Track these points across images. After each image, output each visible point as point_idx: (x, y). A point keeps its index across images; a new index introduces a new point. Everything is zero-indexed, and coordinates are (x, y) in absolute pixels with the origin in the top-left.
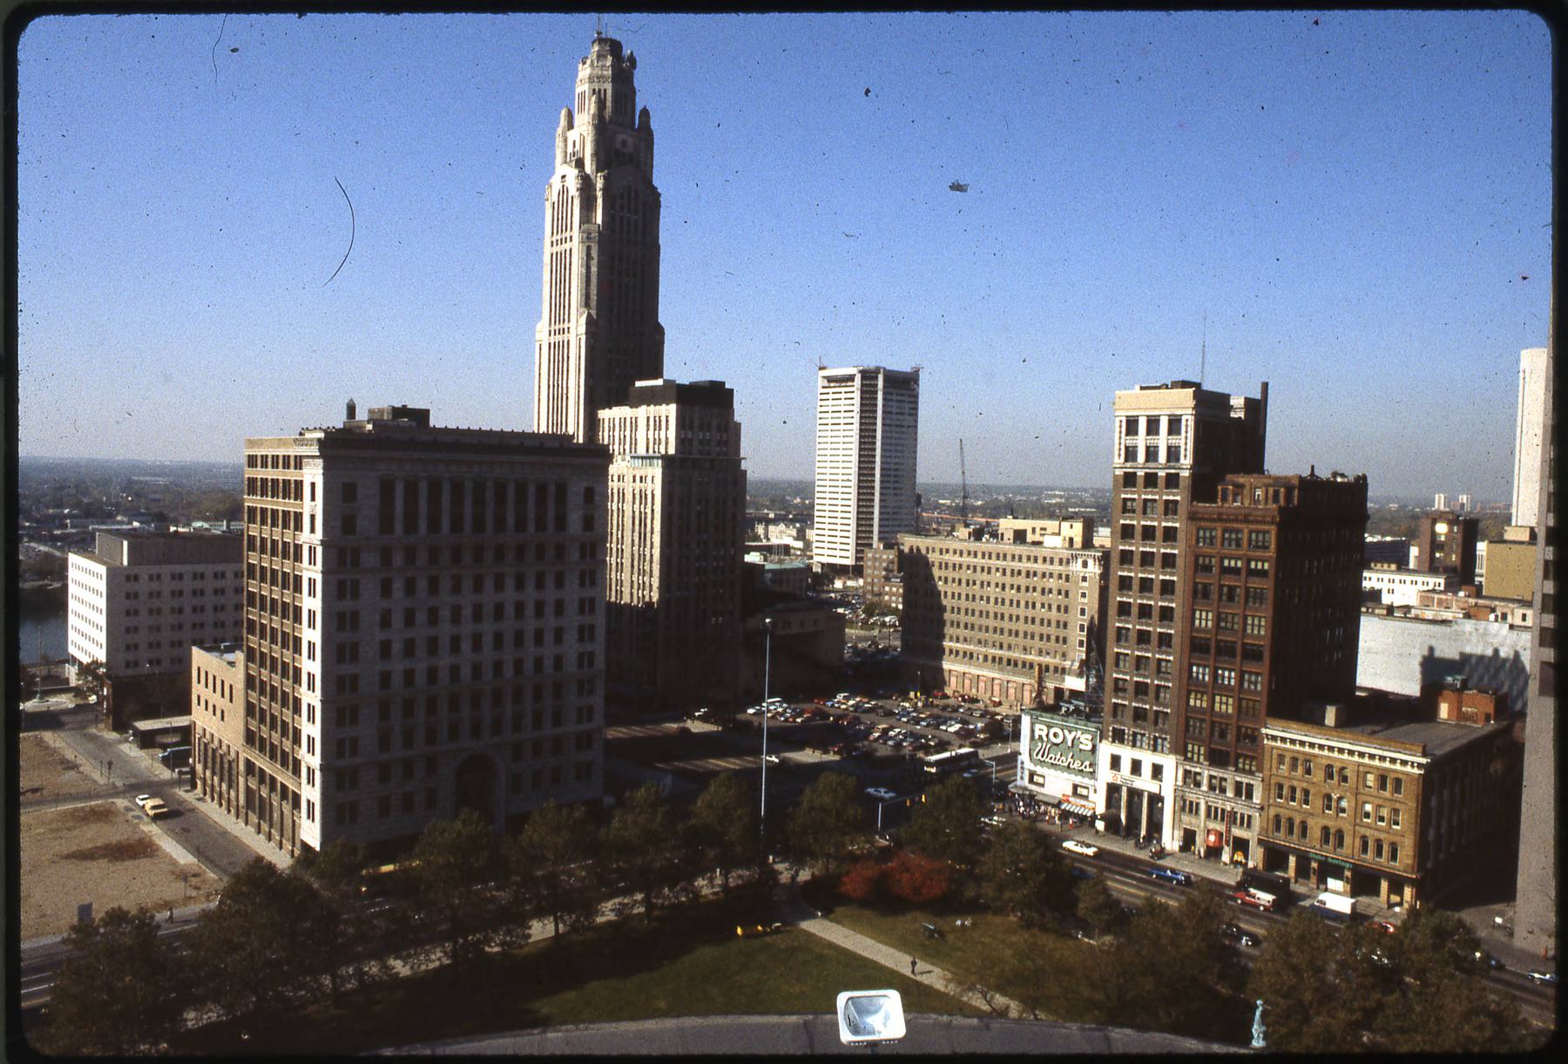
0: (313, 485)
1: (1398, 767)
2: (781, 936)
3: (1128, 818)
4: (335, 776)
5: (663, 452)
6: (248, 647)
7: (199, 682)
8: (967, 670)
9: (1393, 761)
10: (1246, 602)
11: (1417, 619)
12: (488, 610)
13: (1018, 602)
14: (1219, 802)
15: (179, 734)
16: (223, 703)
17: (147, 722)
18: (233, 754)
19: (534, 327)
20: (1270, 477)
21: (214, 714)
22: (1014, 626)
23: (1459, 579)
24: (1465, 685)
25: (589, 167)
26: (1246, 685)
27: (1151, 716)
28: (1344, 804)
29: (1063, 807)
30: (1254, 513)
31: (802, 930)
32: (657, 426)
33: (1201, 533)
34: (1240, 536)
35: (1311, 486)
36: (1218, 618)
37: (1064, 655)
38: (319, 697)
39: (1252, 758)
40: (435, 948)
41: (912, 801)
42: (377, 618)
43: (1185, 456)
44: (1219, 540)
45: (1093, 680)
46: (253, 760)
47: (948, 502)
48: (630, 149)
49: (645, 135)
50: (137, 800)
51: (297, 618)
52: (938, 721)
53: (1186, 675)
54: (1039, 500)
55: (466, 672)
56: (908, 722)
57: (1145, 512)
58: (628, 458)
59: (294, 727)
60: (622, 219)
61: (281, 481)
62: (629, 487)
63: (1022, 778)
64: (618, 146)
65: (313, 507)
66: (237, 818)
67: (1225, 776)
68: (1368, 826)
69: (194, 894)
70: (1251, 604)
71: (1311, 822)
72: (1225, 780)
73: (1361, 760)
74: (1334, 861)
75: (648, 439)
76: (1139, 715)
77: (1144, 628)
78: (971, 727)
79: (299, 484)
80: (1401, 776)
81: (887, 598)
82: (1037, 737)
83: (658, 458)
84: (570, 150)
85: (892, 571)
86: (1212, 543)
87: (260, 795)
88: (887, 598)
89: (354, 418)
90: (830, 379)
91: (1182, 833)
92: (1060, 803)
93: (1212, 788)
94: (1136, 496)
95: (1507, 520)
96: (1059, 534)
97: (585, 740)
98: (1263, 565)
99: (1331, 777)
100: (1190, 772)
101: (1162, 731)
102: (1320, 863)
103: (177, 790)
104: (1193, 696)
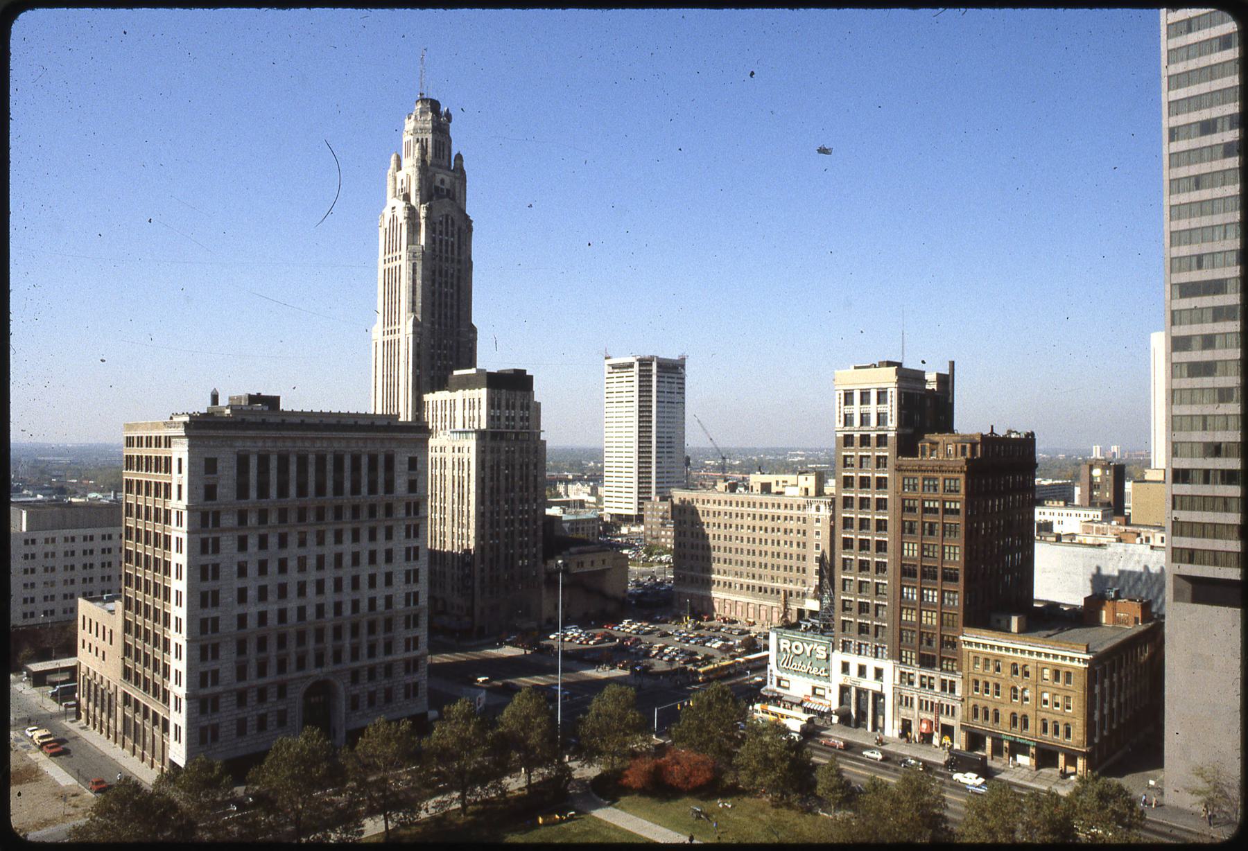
0: (180, 460)
1: (1068, 662)
2: (575, 822)
4: (200, 704)
5: (477, 427)
6: (126, 597)
7: (84, 628)
8: (727, 597)
9: (1064, 658)
10: (944, 535)
11: (1081, 544)
12: (330, 560)
13: (766, 540)
14: (928, 696)
16: (104, 645)
17: (40, 664)
20: (958, 435)
22: (763, 560)
23: (1112, 511)
24: (1118, 596)
25: (414, 201)
26: (946, 601)
27: (872, 630)
28: (1027, 694)
29: (805, 705)
30: (904, 463)
31: (593, 817)
33: (906, 482)
34: (936, 483)
35: (990, 442)
37: (804, 582)
38: (185, 638)
39: (954, 660)
41: (682, 705)
42: (235, 568)
43: (891, 420)
44: (920, 485)
46: (129, 693)
47: (712, 462)
48: (447, 186)
50: (27, 732)
51: (167, 571)
52: (704, 641)
53: (898, 594)
55: (311, 612)
56: (680, 641)
57: (861, 466)
58: (448, 432)
59: (164, 663)
60: (441, 241)
61: (153, 458)
62: (449, 456)
63: (771, 682)
64: (438, 184)
65: (179, 479)
67: (933, 675)
69: (72, 811)
70: (947, 536)
71: (1001, 710)
72: (933, 678)
73: (1039, 659)
74: (1021, 741)
75: (464, 417)
76: (863, 629)
78: (731, 643)
79: (168, 460)
80: (1071, 670)
82: (782, 650)
83: (472, 432)
84: (399, 186)
85: (667, 519)
87: (135, 722)
89: (217, 404)
90: (614, 367)
91: (901, 723)
92: (802, 702)
93: (923, 685)
95: (1148, 465)
96: (797, 485)
97: (412, 666)
98: (955, 506)
99: (1016, 672)
100: (905, 673)
101: (882, 641)
102: (1011, 742)
104: (905, 612)
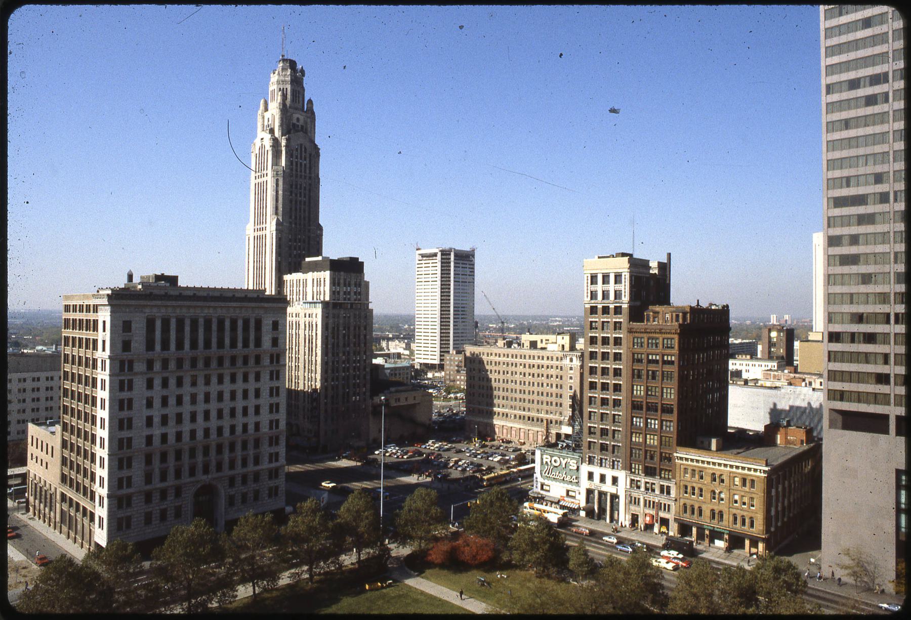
0: (104, 322)
1: (752, 473)
2: (392, 588)
3: (599, 508)
4: (118, 501)
5: (322, 299)
6: (64, 422)
9: (749, 469)
10: (663, 379)
11: (762, 386)
13: (533, 383)
14: (651, 497)
15: (20, 478)
16: (47, 458)
18: (53, 489)
19: (245, 227)
20: (673, 307)
21: (42, 465)
22: (531, 397)
24: (789, 424)
25: (277, 134)
26: (664, 428)
27: (610, 448)
28: (723, 496)
29: (561, 503)
32: (319, 284)
33: (636, 341)
34: (657, 341)
35: (697, 312)
36: (647, 390)
37: (561, 413)
39: (669, 471)
40: (176, 606)
45: (577, 428)
46: (65, 493)
47: (494, 326)
48: (301, 123)
49: (311, 114)
51: (94, 404)
52: (487, 456)
54: (547, 323)
55: (200, 434)
56: (470, 456)
57: (603, 329)
58: (301, 303)
61: (78, 320)
62: (302, 320)
63: (537, 487)
64: (295, 121)
65: (104, 336)
66: (55, 529)
67: (654, 482)
68: (737, 508)
70: (665, 381)
71: (704, 507)
72: (654, 484)
73: (731, 470)
74: (718, 530)
75: (313, 292)
76: (603, 448)
77: (605, 396)
78: (507, 458)
79: (96, 322)
81: (458, 383)
82: (544, 463)
83: (319, 303)
84: (266, 123)
86: (642, 346)
87: (70, 514)
88: (458, 383)
90: (423, 256)
93: (647, 489)
94: (597, 320)
95: (811, 329)
96: (556, 343)
97: (274, 474)
98: (667, 358)
99: (715, 480)
100: (634, 480)
101: (617, 457)
102: (710, 531)
103: (16, 514)
104: (634, 435)
